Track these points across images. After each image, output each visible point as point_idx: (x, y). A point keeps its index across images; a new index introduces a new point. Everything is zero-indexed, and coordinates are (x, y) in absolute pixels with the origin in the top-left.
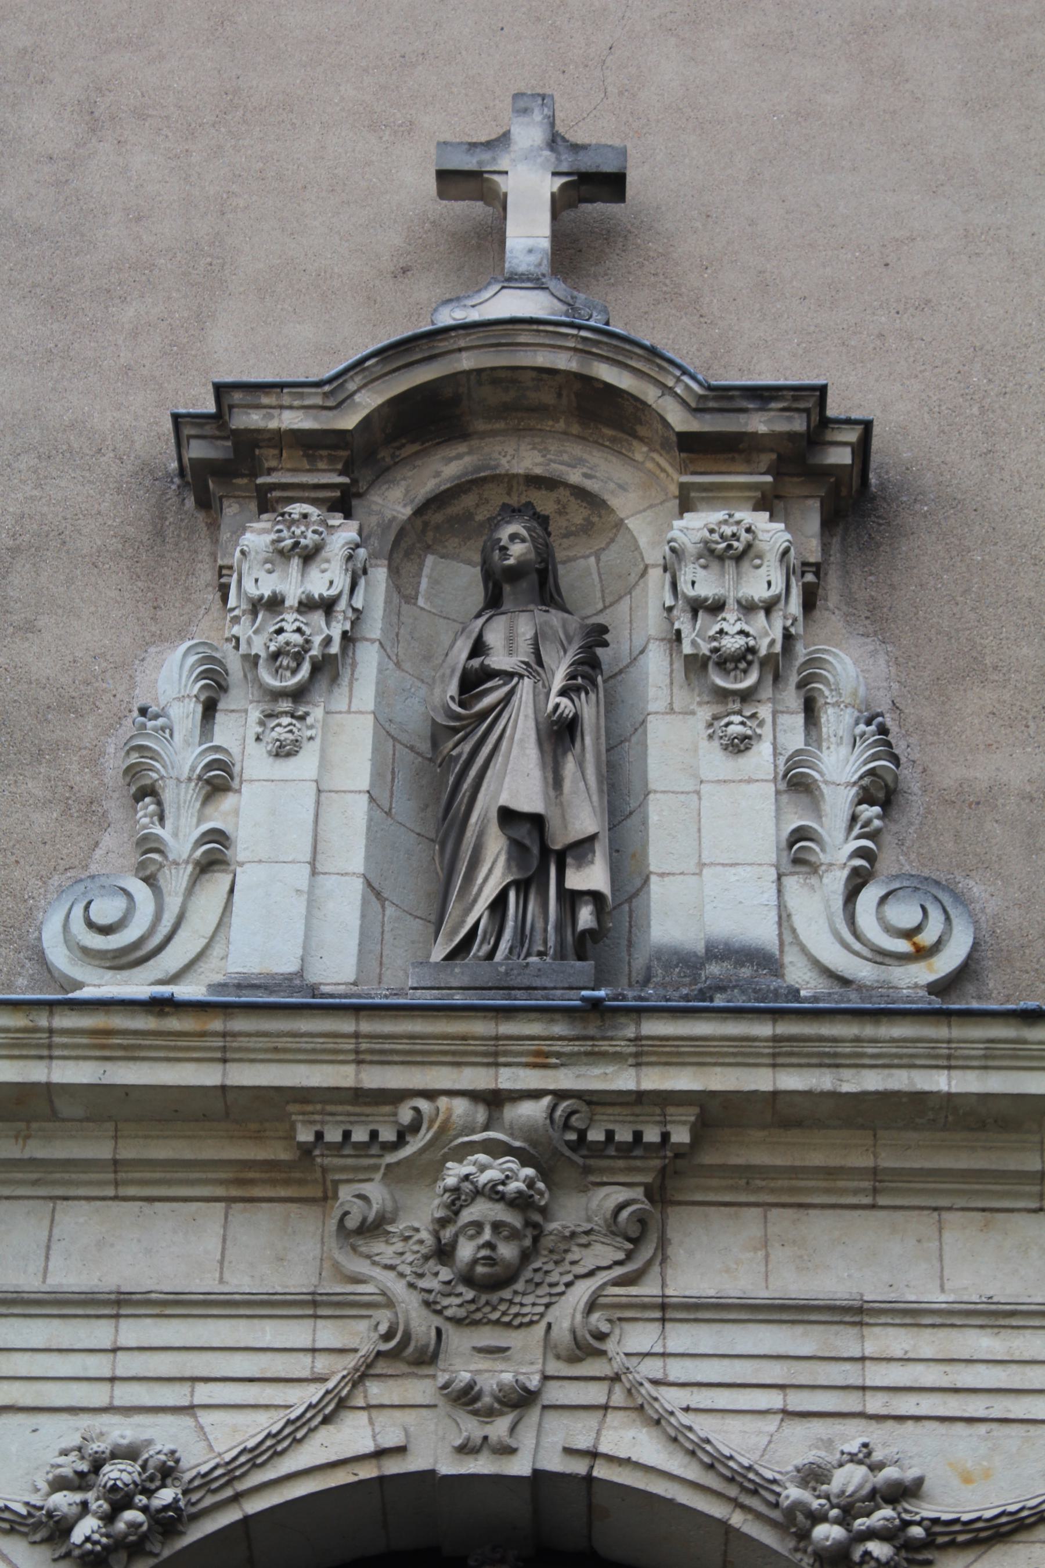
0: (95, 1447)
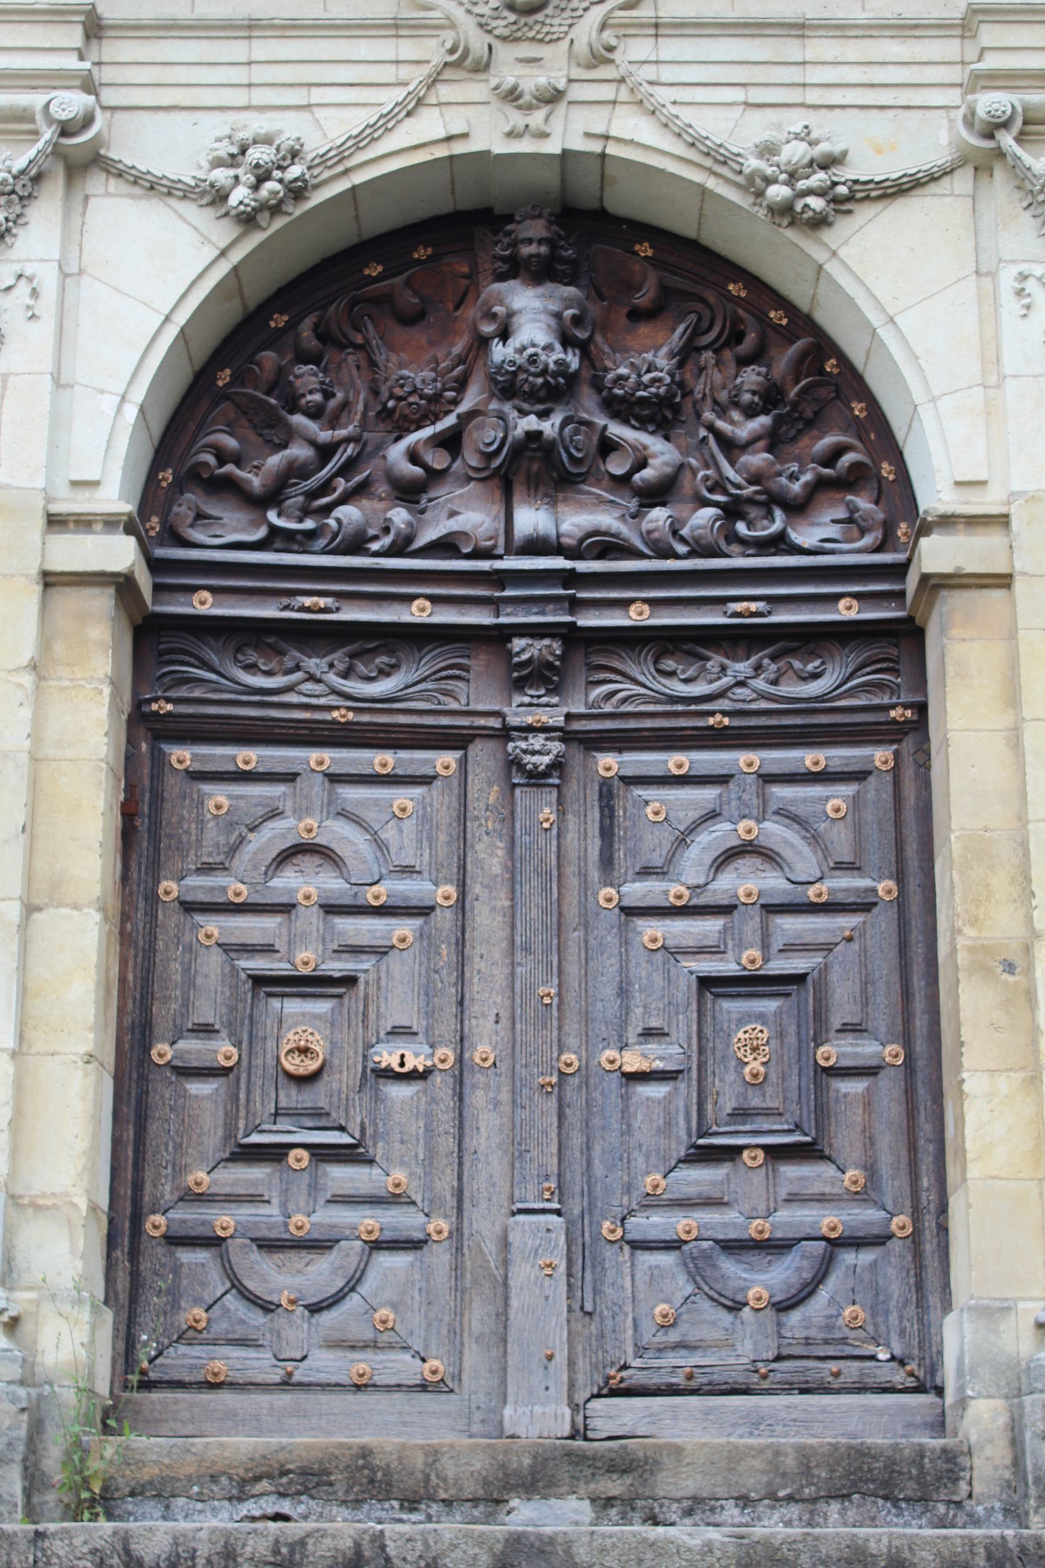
0: (241, 135)
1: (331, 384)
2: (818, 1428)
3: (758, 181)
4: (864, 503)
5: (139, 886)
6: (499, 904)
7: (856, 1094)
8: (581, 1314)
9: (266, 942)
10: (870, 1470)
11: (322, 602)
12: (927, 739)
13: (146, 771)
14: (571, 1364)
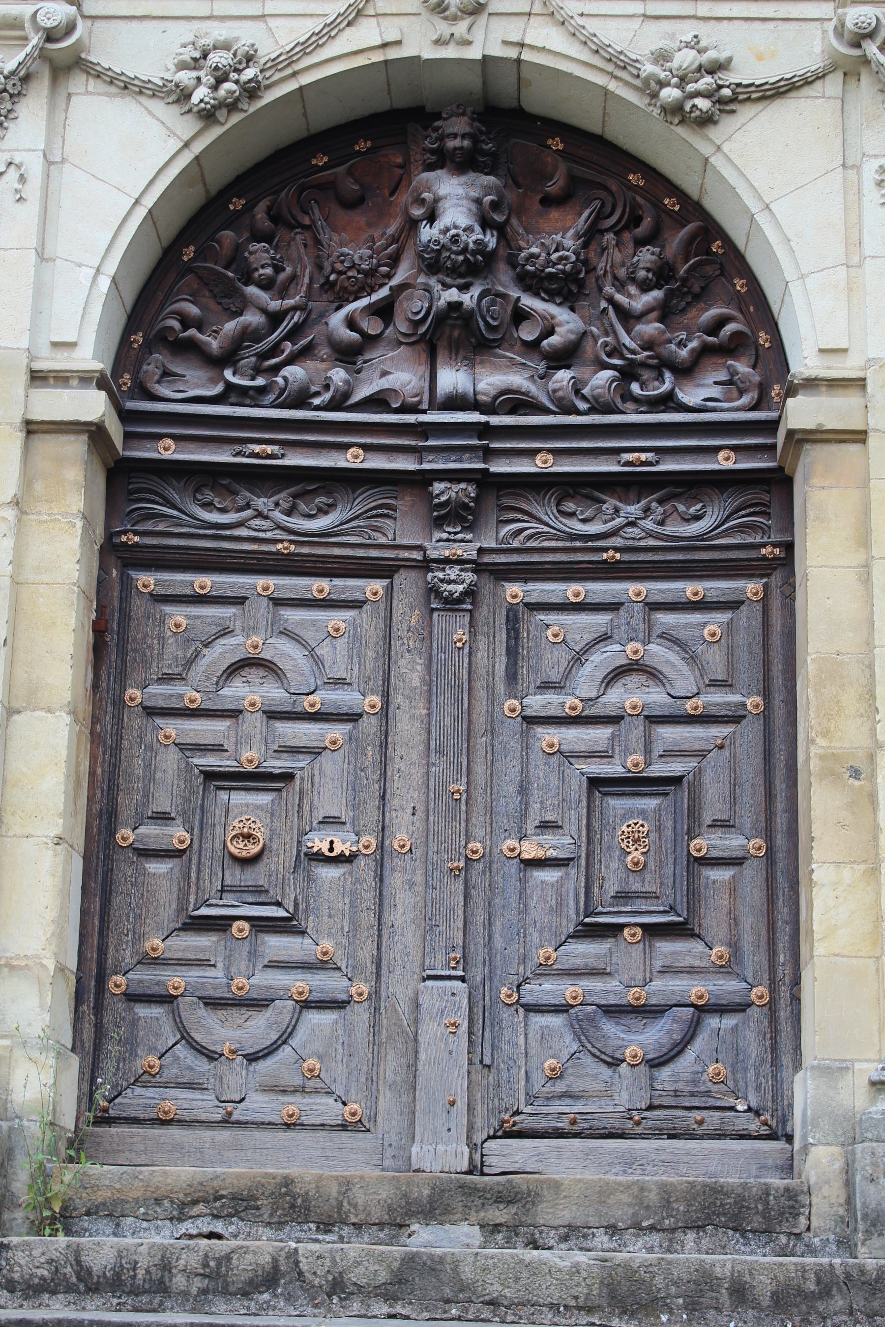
0: (203, 41)
1: (281, 260)
2: (683, 1168)
3: (653, 84)
4: (742, 367)
5: (108, 693)
6: (418, 712)
7: (724, 881)
8: (481, 1066)
9: (216, 742)
10: (722, 1205)
11: (269, 449)
12: (793, 574)
13: (116, 594)
14: (470, 1109)
